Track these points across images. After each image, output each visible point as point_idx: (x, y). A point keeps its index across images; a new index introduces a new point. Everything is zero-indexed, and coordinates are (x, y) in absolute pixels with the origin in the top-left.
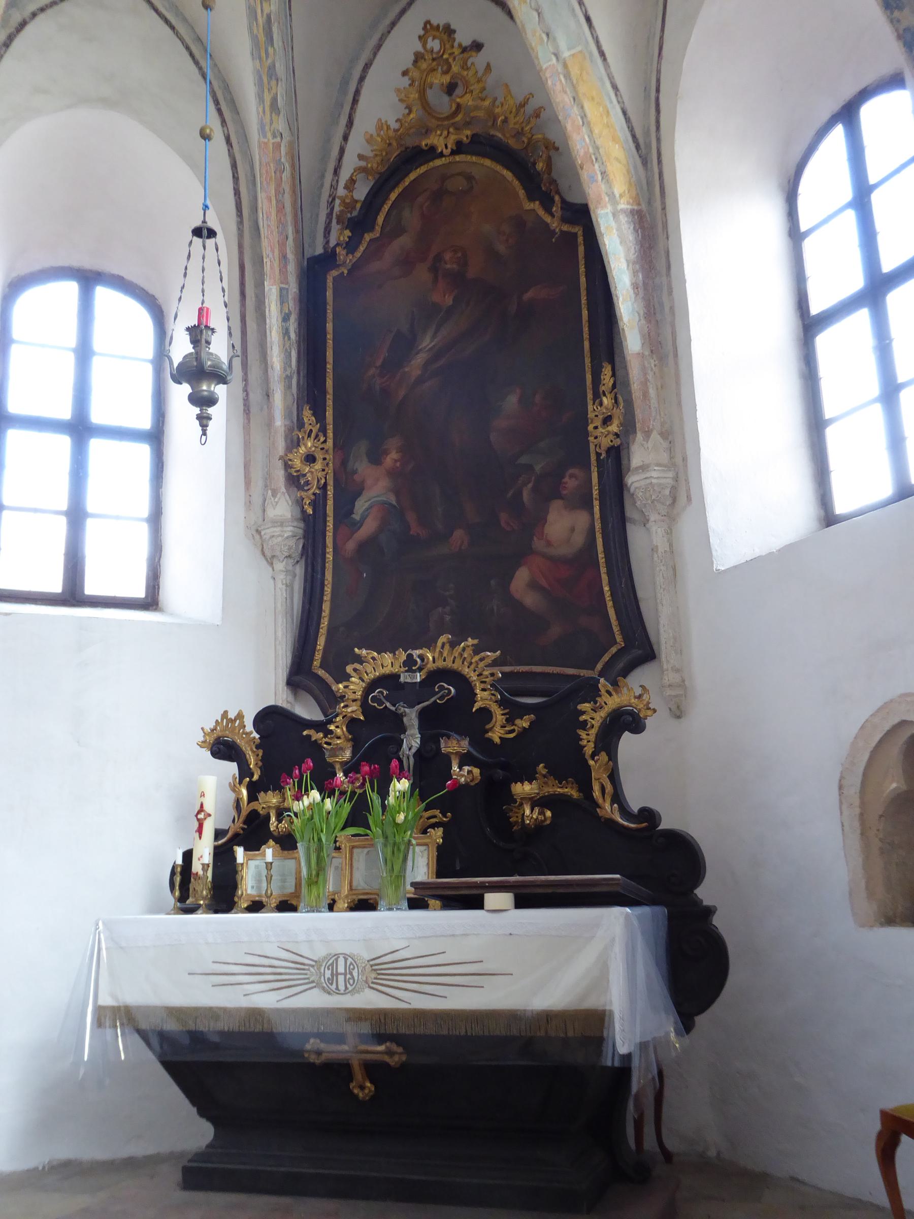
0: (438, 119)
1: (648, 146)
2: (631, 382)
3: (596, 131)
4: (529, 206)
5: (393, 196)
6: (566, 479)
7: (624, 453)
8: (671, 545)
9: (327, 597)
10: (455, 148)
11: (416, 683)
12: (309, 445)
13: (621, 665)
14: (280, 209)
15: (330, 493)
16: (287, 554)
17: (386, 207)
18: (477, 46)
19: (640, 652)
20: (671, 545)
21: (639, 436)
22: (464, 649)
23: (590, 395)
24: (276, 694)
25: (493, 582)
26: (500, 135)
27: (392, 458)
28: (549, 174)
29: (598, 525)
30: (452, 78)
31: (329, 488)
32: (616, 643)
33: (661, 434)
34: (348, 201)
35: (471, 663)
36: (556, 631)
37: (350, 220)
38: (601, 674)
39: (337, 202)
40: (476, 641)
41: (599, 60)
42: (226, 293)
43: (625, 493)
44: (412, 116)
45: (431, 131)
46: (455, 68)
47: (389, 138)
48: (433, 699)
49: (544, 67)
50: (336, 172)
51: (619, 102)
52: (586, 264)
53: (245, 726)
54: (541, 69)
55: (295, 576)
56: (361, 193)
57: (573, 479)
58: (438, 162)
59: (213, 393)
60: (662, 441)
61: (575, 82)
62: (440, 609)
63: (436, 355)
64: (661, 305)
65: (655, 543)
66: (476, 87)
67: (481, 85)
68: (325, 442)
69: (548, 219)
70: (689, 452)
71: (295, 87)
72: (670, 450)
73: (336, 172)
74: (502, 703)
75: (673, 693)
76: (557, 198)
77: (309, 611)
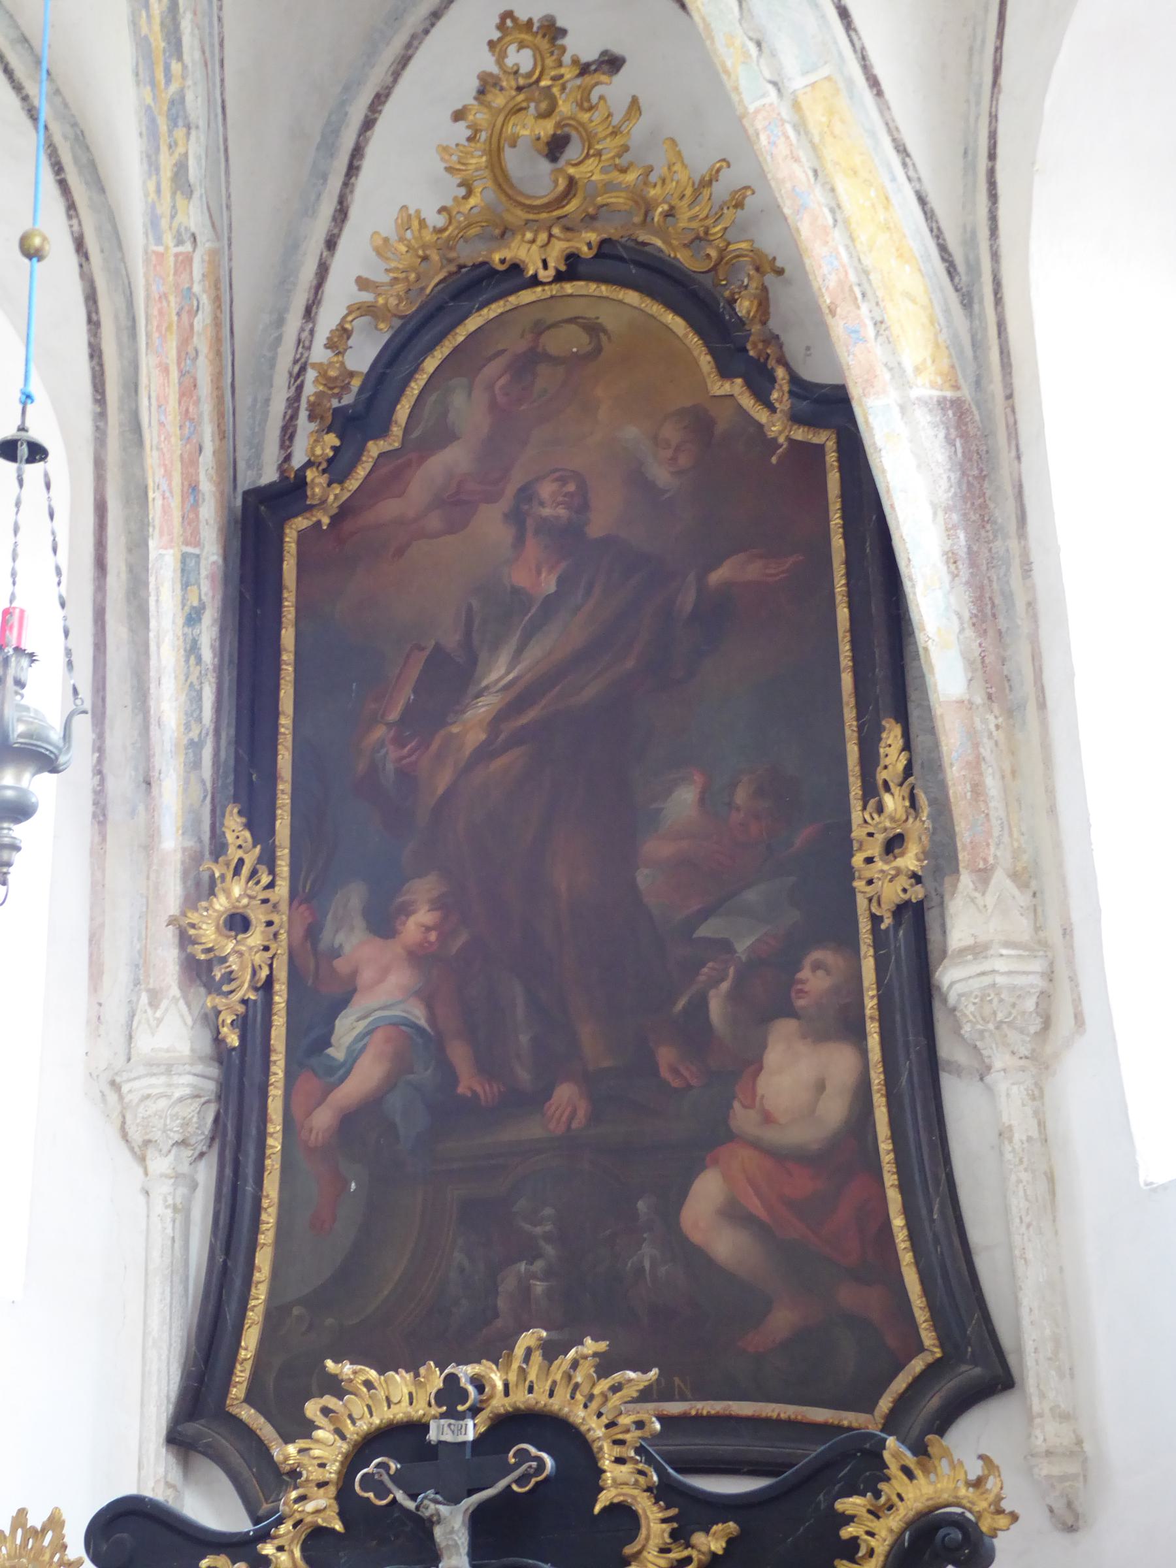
0: (531, 208)
1: (974, 268)
2: (946, 761)
3: (863, 237)
4: (720, 387)
5: (431, 364)
6: (805, 973)
7: (931, 917)
8: (1041, 1125)
9: (266, 1237)
10: (563, 268)
11: (464, 1443)
12: (237, 891)
13: (933, 1402)
14: (188, 390)
15: (280, 1000)
16: (177, 1137)
17: (415, 388)
18: (612, 63)
19: (978, 1371)
20: (1041, 1125)
21: (966, 879)
22: (575, 1364)
23: (855, 789)
24: (141, 1468)
25: (641, 1205)
26: (659, 243)
27: (419, 922)
28: (764, 323)
29: (877, 1078)
30: (558, 125)
31: (277, 987)
32: (921, 1348)
33: (1014, 876)
34: (332, 373)
35: (591, 1397)
36: (783, 1320)
37: (336, 411)
38: (891, 1424)
39: (311, 375)
40: (602, 1346)
41: (868, 95)
42: (64, 579)
43: (937, 1004)
44: (472, 201)
45: (514, 233)
46: (565, 107)
47: (424, 247)
48: (502, 1484)
49: (751, 108)
50: (309, 313)
51: (909, 179)
52: (844, 509)
53: (65, 1547)
54: (745, 114)
55: (194, 1186)
56: (362, 356)
57: (820, 973)
58: (527, 296)
59: (23, 792)
60: (1016, 892)
61: (816, 139)
62: (523, 1266)
63: (520, 700)
64: (1008, 597)
65: (1005, 1119)
66: (609, 146)
67: (619, 141)
68: (271, 885)
69: (761, 415)
70: (1076, 917)
71: (225, 140)
72: (1035, 911)
73: (309, 313)
74: (664, 1492)
75: (1056, 1470)
76: (780, 373)
77: (225, 1271)
